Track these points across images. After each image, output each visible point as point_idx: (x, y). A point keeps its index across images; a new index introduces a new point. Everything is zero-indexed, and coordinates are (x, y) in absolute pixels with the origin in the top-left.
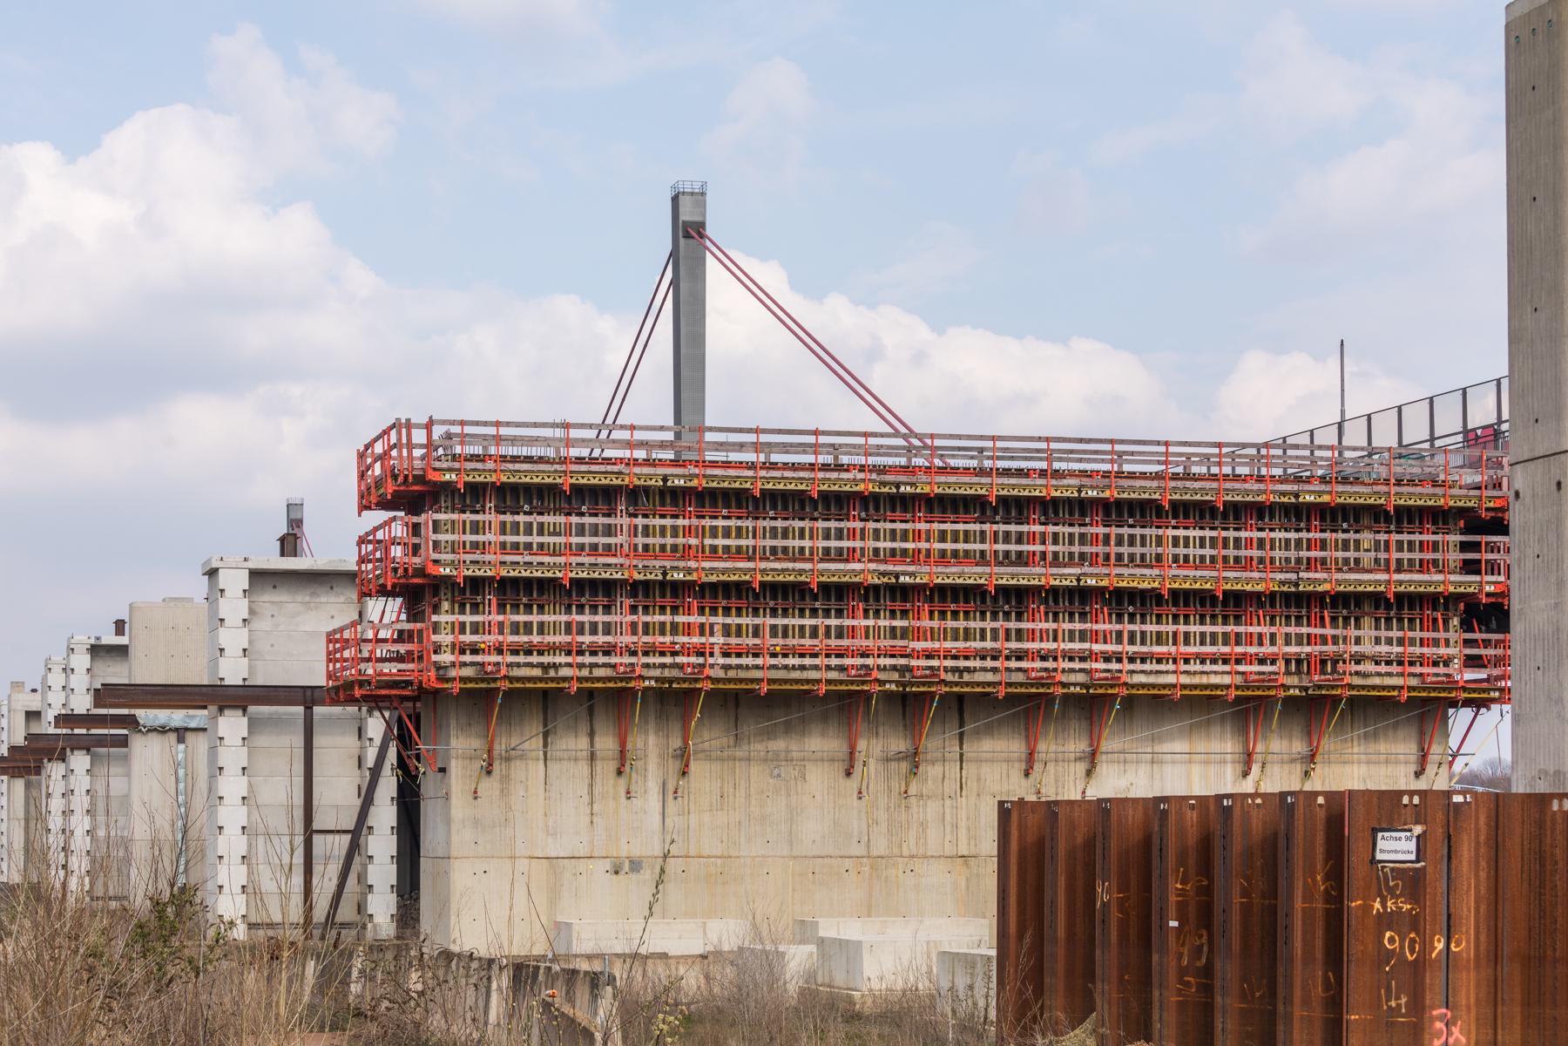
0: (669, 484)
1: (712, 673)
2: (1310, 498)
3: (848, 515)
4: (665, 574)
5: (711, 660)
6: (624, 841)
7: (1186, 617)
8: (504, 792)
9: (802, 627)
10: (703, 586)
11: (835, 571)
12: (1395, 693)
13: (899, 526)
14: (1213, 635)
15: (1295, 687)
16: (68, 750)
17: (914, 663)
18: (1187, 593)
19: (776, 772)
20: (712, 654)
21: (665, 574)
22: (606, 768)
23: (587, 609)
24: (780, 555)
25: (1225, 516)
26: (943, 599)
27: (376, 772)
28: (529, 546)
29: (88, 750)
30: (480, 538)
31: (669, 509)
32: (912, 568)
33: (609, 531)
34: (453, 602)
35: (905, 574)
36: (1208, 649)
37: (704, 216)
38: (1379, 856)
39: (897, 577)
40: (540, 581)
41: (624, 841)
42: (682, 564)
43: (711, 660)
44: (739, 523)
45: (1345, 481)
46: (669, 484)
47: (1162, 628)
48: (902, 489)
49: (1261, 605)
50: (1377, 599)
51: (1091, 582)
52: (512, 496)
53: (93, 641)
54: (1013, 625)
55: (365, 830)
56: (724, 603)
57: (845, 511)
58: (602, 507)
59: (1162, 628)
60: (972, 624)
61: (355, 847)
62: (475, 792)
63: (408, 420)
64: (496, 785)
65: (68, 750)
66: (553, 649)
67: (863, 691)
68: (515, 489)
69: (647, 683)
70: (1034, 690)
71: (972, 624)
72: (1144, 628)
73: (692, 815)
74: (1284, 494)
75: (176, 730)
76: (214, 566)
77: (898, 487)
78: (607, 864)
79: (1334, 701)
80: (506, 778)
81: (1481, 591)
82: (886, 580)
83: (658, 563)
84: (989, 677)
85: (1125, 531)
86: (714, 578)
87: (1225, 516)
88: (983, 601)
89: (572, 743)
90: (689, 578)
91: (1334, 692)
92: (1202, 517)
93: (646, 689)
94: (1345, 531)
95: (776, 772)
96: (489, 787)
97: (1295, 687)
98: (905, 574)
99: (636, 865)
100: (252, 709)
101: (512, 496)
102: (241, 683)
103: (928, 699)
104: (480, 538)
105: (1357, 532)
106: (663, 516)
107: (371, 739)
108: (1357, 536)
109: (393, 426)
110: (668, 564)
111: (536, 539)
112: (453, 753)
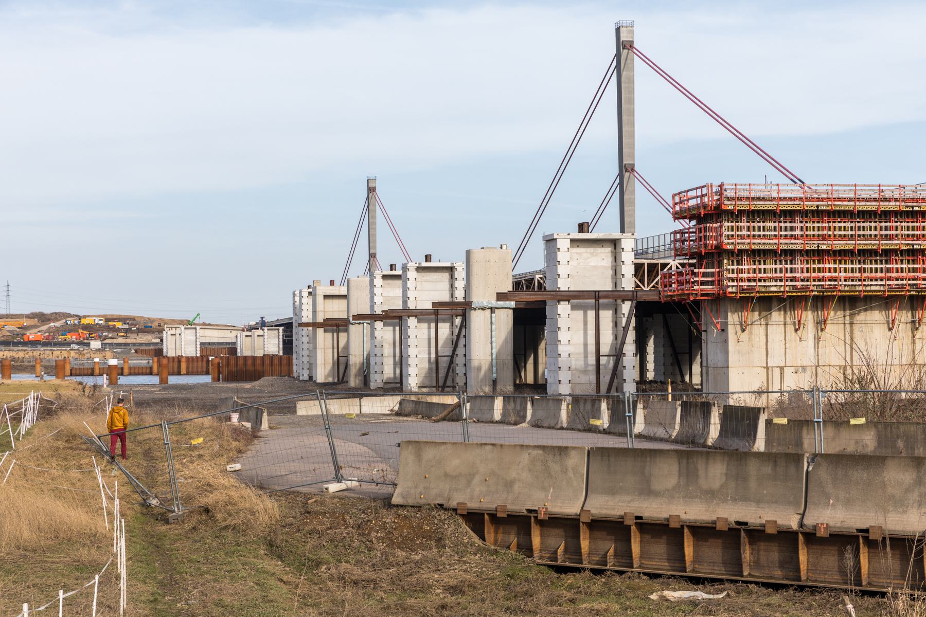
0: (819, 208)
1: (840, 288)
2: (824, 208)
3: (741, 219)
4: (818, 247)
5: (840, 283)
6: (799, 359)
7: (845, 261)
8: (750, 339)
9: (871, 269)
10: (835, 251)
11: (887, 244)
12: (733, 295)
13: (910, 224)
14: (876, 269)
15: (815, 291)
16: (454, 316)
17: (918, 282)
18: (864, 250)
19: (861, 329)
20: (840, 281)
21: (818, 247)
22: (790, 328)
23: (783, 262)
24: (862, 237)
25: (880, 216)
26: (835, 255)
27: (626, 329)
28: (759, 236)
29: (416, 316)
30: (793, 233)
31: (816, 219)
32: (919, 242)
33: (792, 229)
34: (729, 260)
35: (916, 245)
36: (874, 274)
37: (633, 38)
38: (336, 380)
39: (913, 246)
40: (764, 250)
41: (799, 359)
42: (825, 242)
43: (840, 283)
44: (845, 224)
45: (886, 200)
46: (819, 208)
47: (854, 266)
48: (915, 209)
49: (829, 255)
50: (800, 252)
51: (824, 247)
52: (753, 215)
53: (417, 265)
54: (789, 266)
55: (455, 356)
56: (839, 258)
57: (888, 218)
58: (788, 219)
59: (854, 266)
60: (847, 266)
61: (451, 362)
62: (739, 339)
63: (711, 184)
64: (747, 337)
65: (454, 316)
66: (770, 279)
67: (902, 295)
68: (753, 212)
69: (814, 293)
70: (799, 294)
71: (847, 266)
72: (840, 266)
73: (827, 348)
74: (907, 207)
75: (491, 308)
76: (555, 238)
77: (913, 208)
78: (792, 369)
79: (806, 298)
80: (751, 333)
81: (879, 248)
82: (908, 247)
83: (816, 242)
84: (877, 288)
85: (756, 224)
86: (838, 248)
87: (880, 216)
88: (776, 256)
89: (777, 316)
90: (828, 248)
91: (752, 295)
92: (870, 217)
93: (814, 296)
94: (839, 222)
95: (861, 329)
96: (744, 336)
97: (815, 291)
98: (916, 245)
99: (804, 368)
100: (573, 301)
101: (753, 215)
102: (567, 290)
103: (750, 300)
104: (793, 233)
105: (764, 222)
106: (908, 222)
107: (624, 314)
108: (764, 224)
109: (705, 186)
110: (819, 242)
111: (762, 233)
112: (729, 323)
